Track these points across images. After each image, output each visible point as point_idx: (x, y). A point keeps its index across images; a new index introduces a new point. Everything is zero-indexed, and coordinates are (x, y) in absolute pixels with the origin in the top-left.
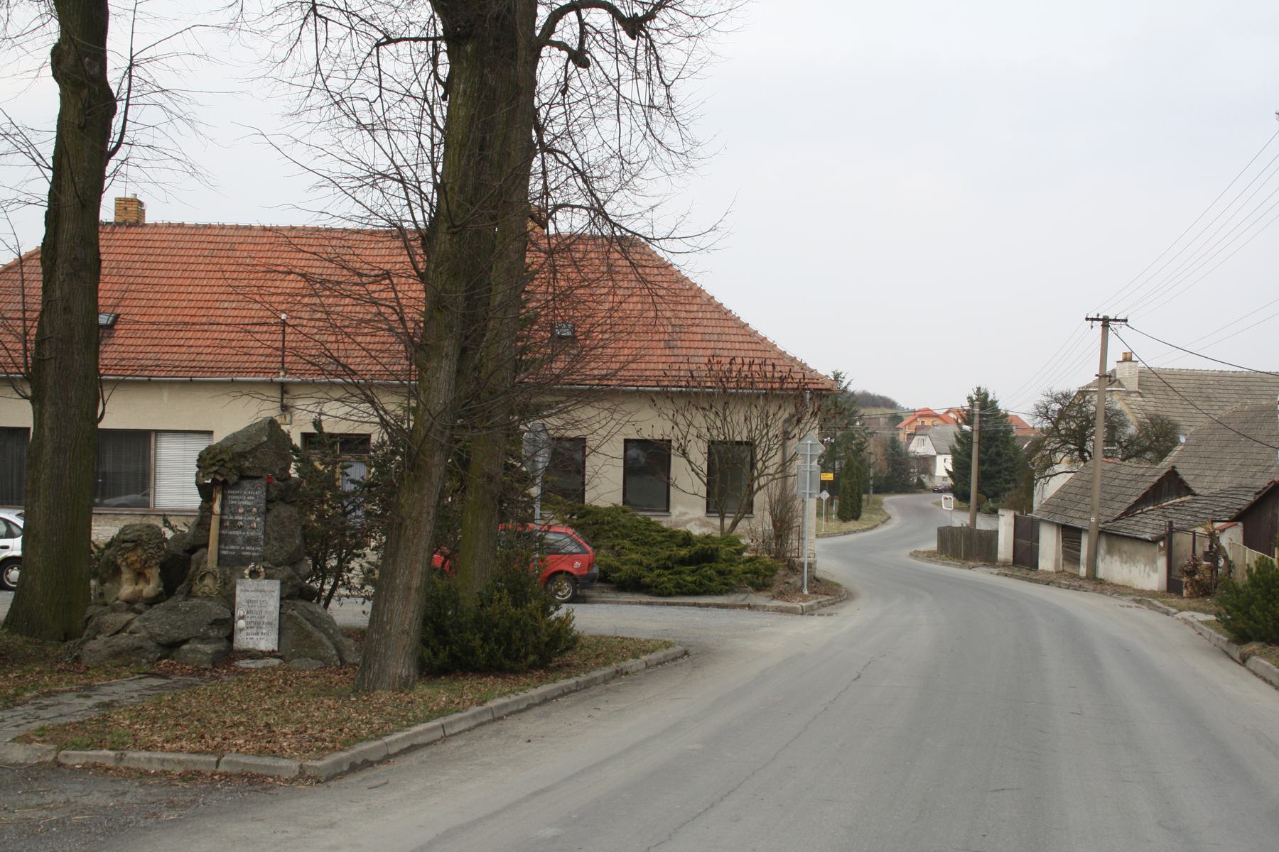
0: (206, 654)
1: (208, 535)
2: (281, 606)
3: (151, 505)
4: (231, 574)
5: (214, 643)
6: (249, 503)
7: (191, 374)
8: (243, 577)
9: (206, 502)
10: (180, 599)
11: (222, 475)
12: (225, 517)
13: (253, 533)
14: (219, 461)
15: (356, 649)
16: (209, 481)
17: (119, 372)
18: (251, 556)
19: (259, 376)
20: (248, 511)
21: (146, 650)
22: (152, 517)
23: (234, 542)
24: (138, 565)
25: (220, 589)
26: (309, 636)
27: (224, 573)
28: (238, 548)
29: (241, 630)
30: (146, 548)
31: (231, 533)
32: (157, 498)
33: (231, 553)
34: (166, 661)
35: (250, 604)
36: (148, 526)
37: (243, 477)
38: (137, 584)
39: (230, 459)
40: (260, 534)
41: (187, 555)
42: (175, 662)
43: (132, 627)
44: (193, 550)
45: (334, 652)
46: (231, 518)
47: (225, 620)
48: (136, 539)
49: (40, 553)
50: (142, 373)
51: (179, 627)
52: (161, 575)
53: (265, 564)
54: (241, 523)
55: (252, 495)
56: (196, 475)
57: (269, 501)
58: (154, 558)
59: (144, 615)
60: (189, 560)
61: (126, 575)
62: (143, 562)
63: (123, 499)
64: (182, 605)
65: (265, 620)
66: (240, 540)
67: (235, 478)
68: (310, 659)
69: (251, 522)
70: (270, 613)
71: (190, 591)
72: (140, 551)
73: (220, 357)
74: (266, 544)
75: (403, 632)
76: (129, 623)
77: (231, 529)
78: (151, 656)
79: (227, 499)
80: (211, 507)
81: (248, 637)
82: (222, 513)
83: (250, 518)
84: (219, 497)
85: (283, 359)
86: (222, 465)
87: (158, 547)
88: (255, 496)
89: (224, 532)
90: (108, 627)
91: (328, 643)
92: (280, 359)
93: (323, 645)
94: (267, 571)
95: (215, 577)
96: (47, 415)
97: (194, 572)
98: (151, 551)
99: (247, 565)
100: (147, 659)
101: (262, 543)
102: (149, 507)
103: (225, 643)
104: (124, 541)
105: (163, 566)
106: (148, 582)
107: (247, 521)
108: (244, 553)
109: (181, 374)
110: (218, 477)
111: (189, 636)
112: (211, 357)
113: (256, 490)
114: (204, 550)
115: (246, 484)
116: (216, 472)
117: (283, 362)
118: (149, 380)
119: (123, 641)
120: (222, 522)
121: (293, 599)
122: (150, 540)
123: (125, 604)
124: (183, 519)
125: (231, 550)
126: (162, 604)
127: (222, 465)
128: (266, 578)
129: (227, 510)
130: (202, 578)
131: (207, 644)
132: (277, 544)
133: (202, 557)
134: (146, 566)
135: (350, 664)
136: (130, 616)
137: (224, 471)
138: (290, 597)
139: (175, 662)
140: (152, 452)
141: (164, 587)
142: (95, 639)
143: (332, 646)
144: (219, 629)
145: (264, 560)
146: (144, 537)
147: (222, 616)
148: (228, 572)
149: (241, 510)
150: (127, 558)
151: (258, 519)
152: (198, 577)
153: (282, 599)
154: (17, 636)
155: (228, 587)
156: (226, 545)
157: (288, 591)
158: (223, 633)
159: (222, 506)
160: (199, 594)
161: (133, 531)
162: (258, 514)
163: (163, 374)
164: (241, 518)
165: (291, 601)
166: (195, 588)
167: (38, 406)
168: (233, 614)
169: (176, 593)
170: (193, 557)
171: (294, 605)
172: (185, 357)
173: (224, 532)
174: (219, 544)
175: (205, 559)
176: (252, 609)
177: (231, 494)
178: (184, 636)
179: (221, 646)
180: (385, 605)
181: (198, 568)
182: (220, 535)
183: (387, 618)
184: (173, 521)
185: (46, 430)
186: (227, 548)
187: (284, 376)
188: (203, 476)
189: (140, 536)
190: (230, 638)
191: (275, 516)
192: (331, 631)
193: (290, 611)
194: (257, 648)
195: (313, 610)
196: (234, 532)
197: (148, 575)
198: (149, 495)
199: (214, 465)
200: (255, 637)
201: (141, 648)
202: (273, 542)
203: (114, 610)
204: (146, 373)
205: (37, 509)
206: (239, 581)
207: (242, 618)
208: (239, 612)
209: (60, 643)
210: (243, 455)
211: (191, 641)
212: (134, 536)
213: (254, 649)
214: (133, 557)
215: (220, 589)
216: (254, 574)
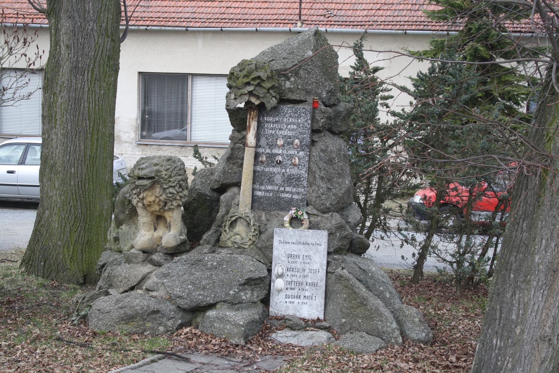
0: (237, 325)
1: (241, 172)
2: (328, 263)
3: (188, 138)
4: (268, 220)
5: (247, 308)
6: (290, 134)
7: (221, 25)
8: (282, 225)
9: (239, 131)
10: (206, 250)
11: (258, 97)
12: (260, 150)
13: (295, 171)
14: (254, 79)
15: (420, 321)
16: (242, 105)
17: (162, 23)
18: (292, 199)
19: (279, 27)
20: (289, 143)
21: (164, 316)
22: (189, 148)
23: (271, 181)
24: (156, 208)
25: (254, 239)
26: (363, 303)
27: (259, 219)
28: (276, 188)
29: (280, 291)
30: (165, 186)
31: (267, 170)
32: (193, 133)
33: (267, 194)
34: (188, 329)
35: (290, 260)
36: (169, 160)
37: (283, 101)
38: (155, 229)
39: (268, 78)
40: (303, 172)
41: (215, 195)
42: (198, 332)
43: (149, 283)
44: (222, 189)
45: (394, 325)
46: (268, 151)
47: (261, 279)
48: (153, 175)
49: (57, 186)
50: (181, 24)
51: (204, 288)
52: (183, 218)
53: (310, 209)
54: (280, 158)
55: (294, 124)
56: (227, 97)
57: (315, 132)
58: (175, 199)
59: (163, 270)
60: (218, 200)
61: (143, 218)
62: (162, 204)
63: (165, 134)
64: (210, 259)
65: (309, 280)
66: (278, 179)
67: (274, 102)
68: (364, 334)
69: (291, 157)
70: (316, 271)
71: (218, 240)
72: (158, 190)
73: (246, 11)
74: (310, 184)
75: (543, 338)
76: (144, 278)
77: (268, 165)
78: (170, 323)
79: (263, 127)
80: (244, 138)
81: (288, 300)
82: (258, 146)
83: (291, 152)
84: (253, 125)
85: (300, 11)
86: (259, 85)
87: (180, 186)
88: (298, 125)
89: (258, 168)
90: (121, 282)
91: (386, 312)
92: (298, 11)
93: (381, 315)
94: (312, 219)
95: (249, 224)
96: (63, 31)
97: (223, 217)
98: (171, 190)
99: (287, 209)
100: (165, 326)
101: (305, 183)
102: (186, 140)
103: (260, 307)
104: (140, 178)
105: (187, 206)
106: (168, 227)
107: (287, 156)
108: (283, 195)
109: (213, 25)
110: (253, 100)
111: (217, 300)
112: (238, 11)
113: (299, 117)
114: (235, 189)
115: (287, 108)
116: (251, 93)
117: (300, 15)
118: (187, 30)
119: (137, 301)
120: (257, 156)
121: (341, 254)
122: (170, 177)
123: (142, 254)
124: (214, 152)
125: (268, 191)
126: (184, 257)
127: (259, 85)
128: (310, 228)
129: (263, 141)
130: (233, 224)
131: (238, 310)
132: (324, 186)
133: (233, 198)
134: (166, 208)
135: (413, 341)
136: (147, 268)
137: (261, 92)
138: (338, 251)
139: (198, 332)
140: (189, 93)
141: (188, 234)
142: (107, 294)
143: (390, 316)
144: (252, 290)
145: (307, 205)
146: (164, 173)
147: (257, 275)
148: (263, 218)
149: (280, 142)
150: (143, 199)
151: (301, 154)
152: (228, 223)
153: (329, 253)
154: (32, 277)
155: (263, 237)
156: (261, 184)
157: (336, 244)
158: (257, 294)
159: (258, 137)
160: (229, 244)
161: (150, 166)
162: (301, 147)
163: (198, 25)
164: (280, 152)
165: (340, 257)
166: (224, 237)
167: (53, 20)
168: (270, 271)
169: (201, 242)
170: (222, 197)
171: (344, 261)
172: (216, 10)
173: (258, 168)
174: (254, 183)
175: (236, 201)
176: (293, 265)
177: (267, 122)
178: (210, 300)
179: (254, 313)
180: (514, 294)
181: (227, 212)
182: (255, 172)
183: (518, 315)
184: (204, 153)
185: (63, 48)
186: (263, 188)
187: (301, 27)
188: (235, 99)
189: (158, 171)
190: (266, 301)
191: (322, 151)
192: (388, 295)
193: (339, 270)
194: (298, 315)
195: (365, 268)
196: (271, 169)
197: (168, 220)
198: (186, 130)
199: (248, 84)
200: (296, 301)
201: (158, 312)
202: (319, 182)
203: (128, 260)
204: (184, 24)
205: (54, 137)
206: (277, 230)
207: (281, 276)
208: (277, 269)
209: (78, 287)
210: (282, 74)
211: (218, 306)
212: (151, 172)
213: (294, 316)
214: (150, 197)
215: (254, 239)
216: (295, 221)
